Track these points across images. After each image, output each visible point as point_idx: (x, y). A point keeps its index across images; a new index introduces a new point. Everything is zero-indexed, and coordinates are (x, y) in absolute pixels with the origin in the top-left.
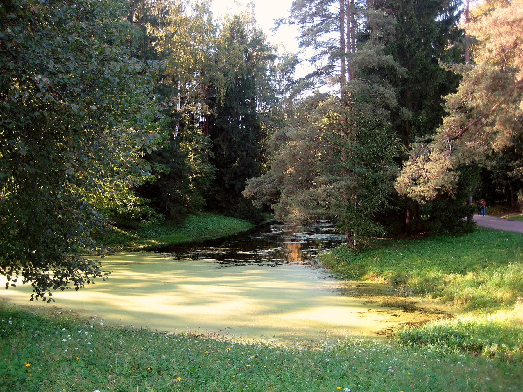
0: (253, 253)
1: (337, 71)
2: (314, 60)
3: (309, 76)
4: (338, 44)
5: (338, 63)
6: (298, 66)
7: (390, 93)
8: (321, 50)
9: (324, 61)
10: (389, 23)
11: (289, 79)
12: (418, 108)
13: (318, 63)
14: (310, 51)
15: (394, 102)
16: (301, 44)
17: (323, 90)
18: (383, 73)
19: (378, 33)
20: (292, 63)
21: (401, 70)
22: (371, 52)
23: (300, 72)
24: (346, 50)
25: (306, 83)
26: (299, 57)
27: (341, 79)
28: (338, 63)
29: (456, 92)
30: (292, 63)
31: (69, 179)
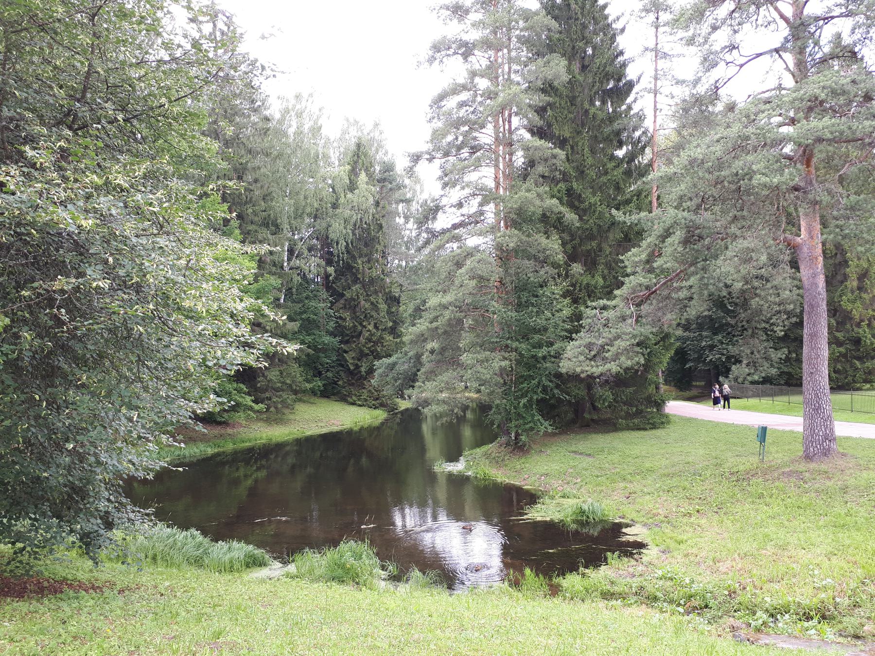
0: (501, 175)
1: (490, 217)
2: (460, 205)
3: (455, 227)
4: (491, 184)
5: (490, 208)
6: (440, 215)
7: (553, 245)
8: (467, 191)
9: (472, 207)
10: (554, 156)
11: (429, 231)
12: (591, 265)
13: (465, 210)
14: (456, 194)
15: (560, 258)
16: (445, 185)
17: (472, 242)
18: (549, 222)
19: (540, 169)
20: (432, 211)
21: (570, 217)
22: (540, 199)
23: (442, 222)
24: (501, 191)
25: (452, 233)
26: (444, 201)
27: (493, 229)
28: (490, 208)
29: (640, 246)
30: (432, 211)
31: (589, 129)
